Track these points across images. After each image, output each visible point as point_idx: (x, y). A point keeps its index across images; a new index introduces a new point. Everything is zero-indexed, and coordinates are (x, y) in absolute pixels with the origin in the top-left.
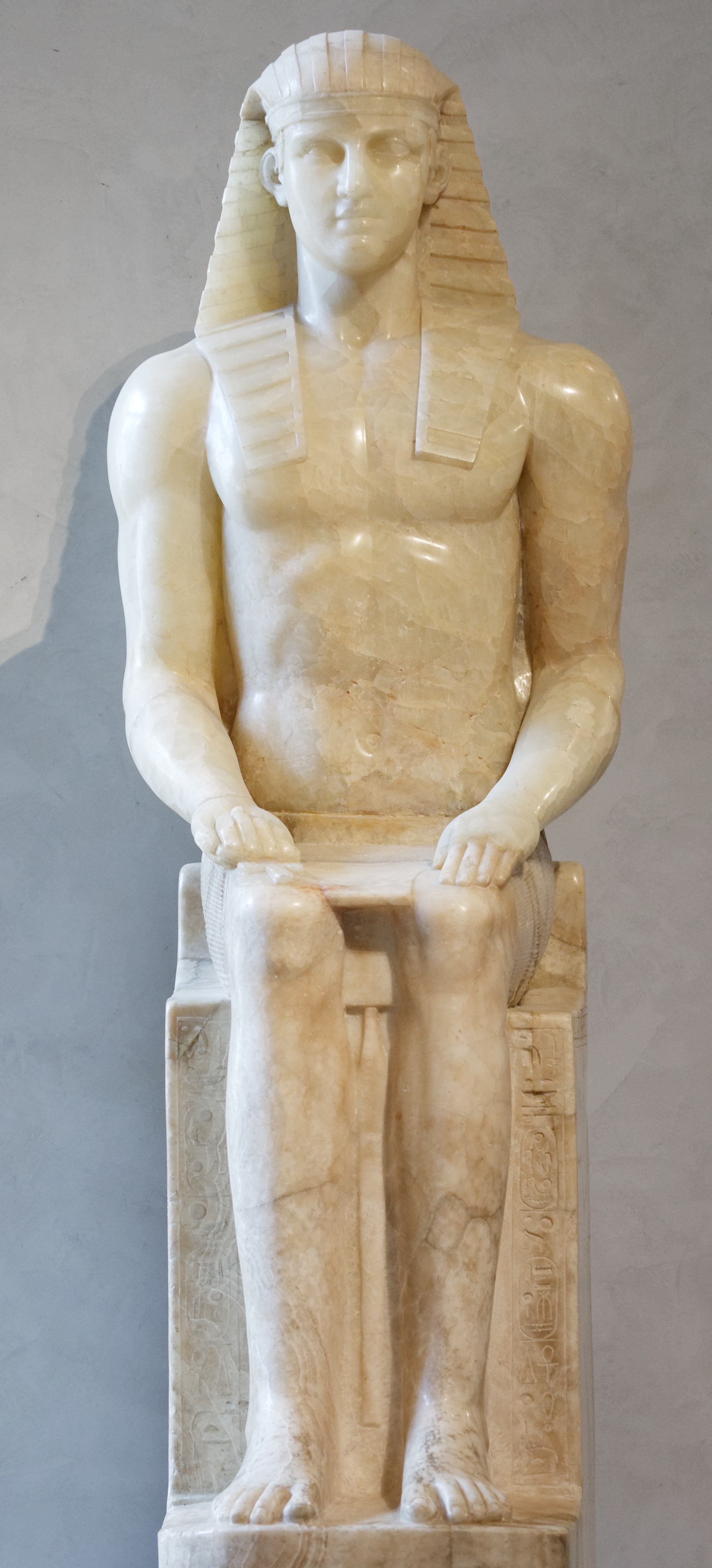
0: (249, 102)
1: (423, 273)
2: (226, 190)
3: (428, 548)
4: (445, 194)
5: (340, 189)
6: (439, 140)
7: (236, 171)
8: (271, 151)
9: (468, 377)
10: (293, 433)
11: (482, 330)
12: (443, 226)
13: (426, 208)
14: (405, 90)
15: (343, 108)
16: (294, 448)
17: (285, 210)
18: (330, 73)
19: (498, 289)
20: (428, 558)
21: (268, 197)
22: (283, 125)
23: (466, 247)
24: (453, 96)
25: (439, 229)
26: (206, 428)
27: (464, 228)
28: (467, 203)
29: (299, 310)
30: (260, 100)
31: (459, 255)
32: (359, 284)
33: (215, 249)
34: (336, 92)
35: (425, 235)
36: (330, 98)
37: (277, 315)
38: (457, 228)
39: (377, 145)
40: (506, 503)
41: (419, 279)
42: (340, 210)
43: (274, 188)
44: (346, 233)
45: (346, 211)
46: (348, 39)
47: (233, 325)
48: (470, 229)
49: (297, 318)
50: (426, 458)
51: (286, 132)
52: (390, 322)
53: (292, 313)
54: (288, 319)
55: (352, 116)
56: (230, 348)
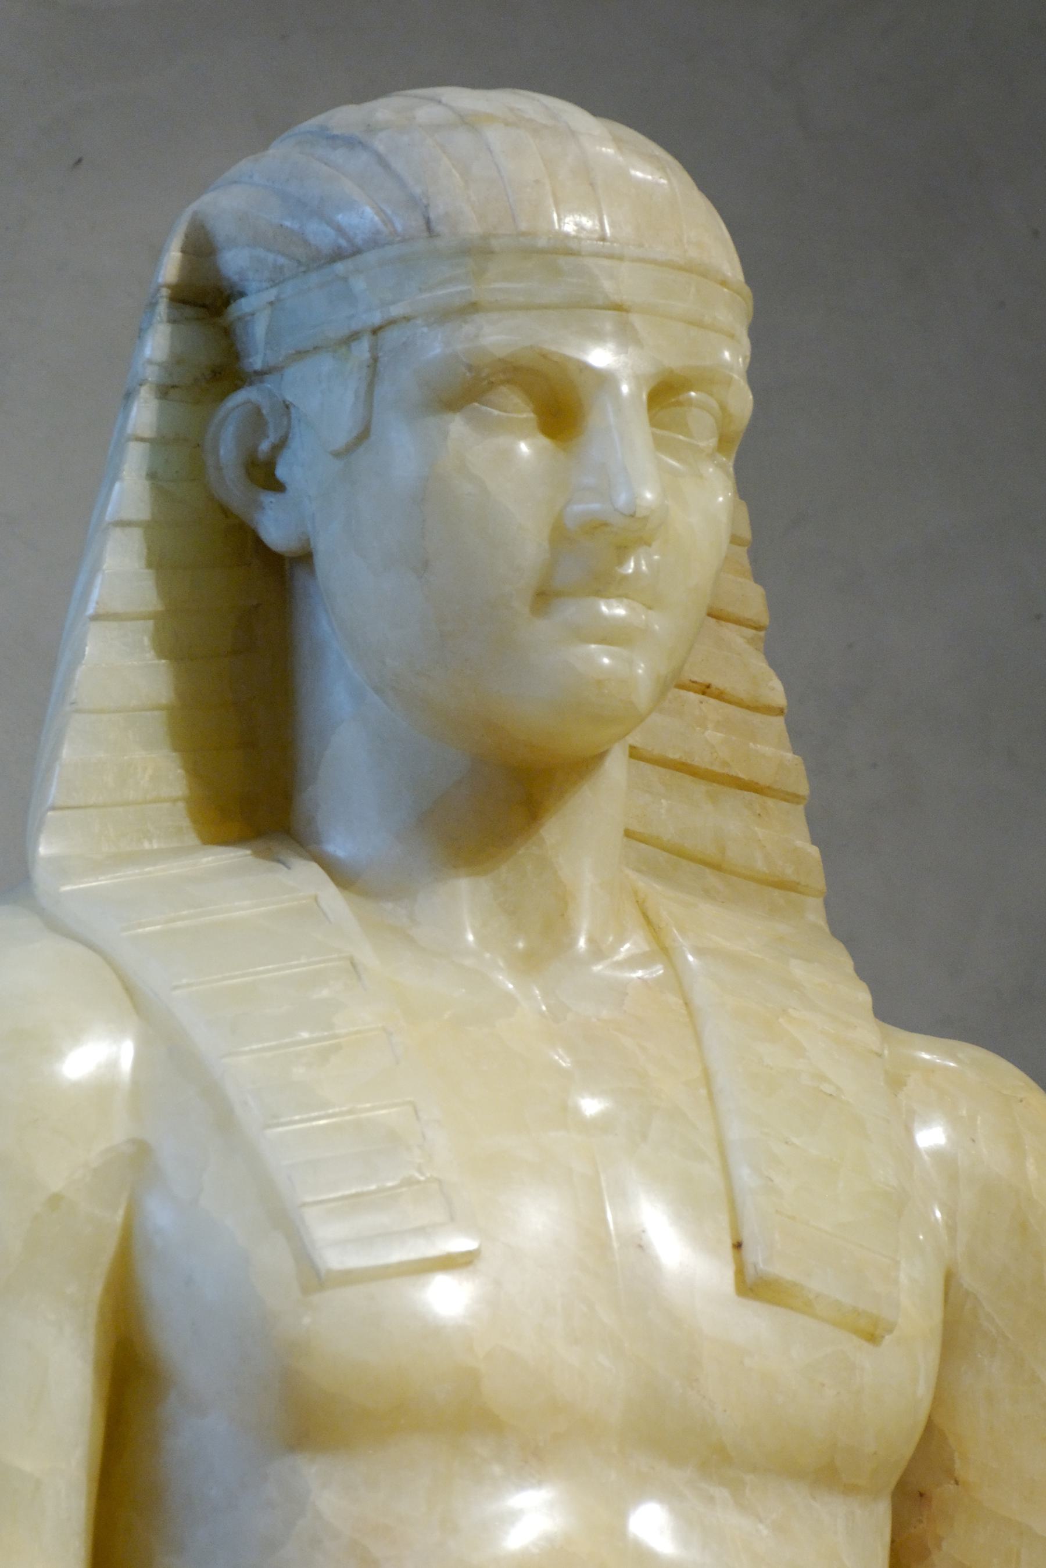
19: (790, 872)
27: (705, 690)
43: (261, 507)
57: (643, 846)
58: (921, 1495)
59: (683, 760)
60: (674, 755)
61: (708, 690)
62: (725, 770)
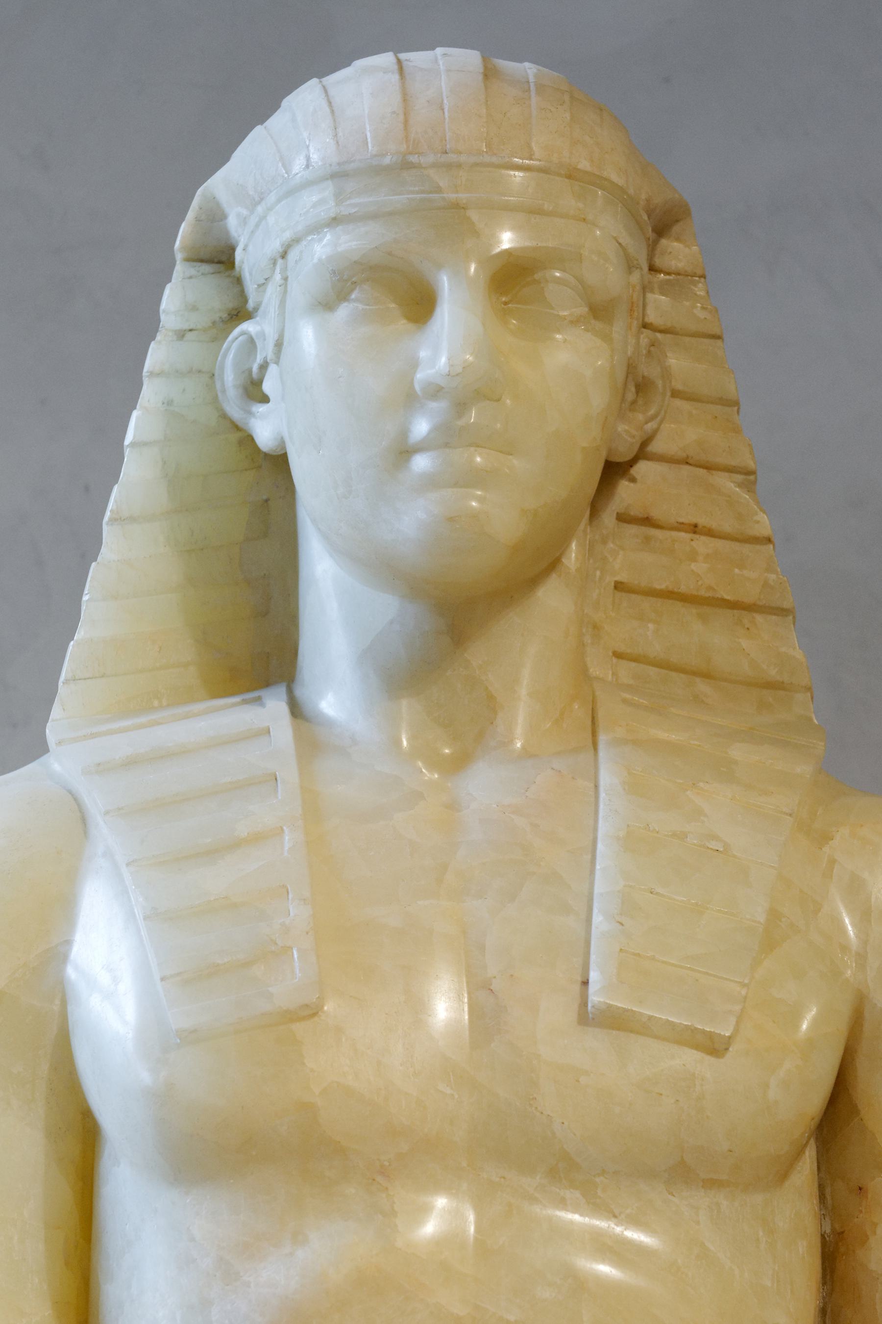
0: (198, 220)
1: (595, 627)
2: (135, 414)
3: (607, 1242)
4: (656, 447)
5: (421, 376)
6: (645, 326)
7: (160, 374)
8: (248, 326)
9: (713, 845)
10: (288, 949)
11: (738, 752)
12: (647, 521)
13: (613, 471)
14: (584, 165)
15: (438, 190)
16: (289, 983)
17: (278, 463)
18: (406, 114)
19: (773, 673)
20: (605, 1269)
21: (234, 437)
22: (288, 235)
23: (699, 566)
24: (676, 229)
25: (632, 530)
26: (68, 943)
27: (694, 529)
28: (702, 472)
29: (299, 692)
30: (224, 217)
31: (683, 589)
32: (454, 616)
33: (103, 550)
34: (420, 154)
35: (604, 542)
36: (406, 165)
37: (245, 702)
38: (680, 527)
39: (512, 282)
40: (809, 1139)
41: (588, 639)
42: (421, 427)
43: (250, 413)
44: (430, 482)
45: (435, 429)
46: (446, 69)
47: (143, 720)
48: (710, 533)
49: (296, 710)
50: (614, 1021)
51: (292, 255)
52: (519, 724)
53: (284, 696)
54: (274, 707)
55: (457, 207)
56: (131, 763)
57: (633, 664)
58: (860, 1189)
59: (670, 588)
60: (660, 585)
61: (696, 529)
62: (710, 594)
